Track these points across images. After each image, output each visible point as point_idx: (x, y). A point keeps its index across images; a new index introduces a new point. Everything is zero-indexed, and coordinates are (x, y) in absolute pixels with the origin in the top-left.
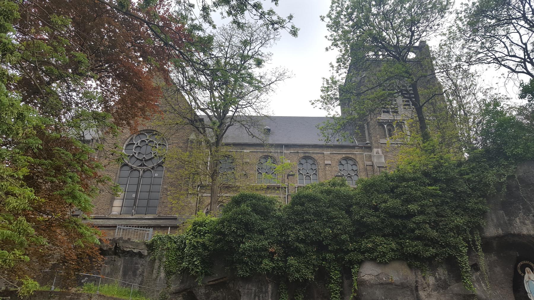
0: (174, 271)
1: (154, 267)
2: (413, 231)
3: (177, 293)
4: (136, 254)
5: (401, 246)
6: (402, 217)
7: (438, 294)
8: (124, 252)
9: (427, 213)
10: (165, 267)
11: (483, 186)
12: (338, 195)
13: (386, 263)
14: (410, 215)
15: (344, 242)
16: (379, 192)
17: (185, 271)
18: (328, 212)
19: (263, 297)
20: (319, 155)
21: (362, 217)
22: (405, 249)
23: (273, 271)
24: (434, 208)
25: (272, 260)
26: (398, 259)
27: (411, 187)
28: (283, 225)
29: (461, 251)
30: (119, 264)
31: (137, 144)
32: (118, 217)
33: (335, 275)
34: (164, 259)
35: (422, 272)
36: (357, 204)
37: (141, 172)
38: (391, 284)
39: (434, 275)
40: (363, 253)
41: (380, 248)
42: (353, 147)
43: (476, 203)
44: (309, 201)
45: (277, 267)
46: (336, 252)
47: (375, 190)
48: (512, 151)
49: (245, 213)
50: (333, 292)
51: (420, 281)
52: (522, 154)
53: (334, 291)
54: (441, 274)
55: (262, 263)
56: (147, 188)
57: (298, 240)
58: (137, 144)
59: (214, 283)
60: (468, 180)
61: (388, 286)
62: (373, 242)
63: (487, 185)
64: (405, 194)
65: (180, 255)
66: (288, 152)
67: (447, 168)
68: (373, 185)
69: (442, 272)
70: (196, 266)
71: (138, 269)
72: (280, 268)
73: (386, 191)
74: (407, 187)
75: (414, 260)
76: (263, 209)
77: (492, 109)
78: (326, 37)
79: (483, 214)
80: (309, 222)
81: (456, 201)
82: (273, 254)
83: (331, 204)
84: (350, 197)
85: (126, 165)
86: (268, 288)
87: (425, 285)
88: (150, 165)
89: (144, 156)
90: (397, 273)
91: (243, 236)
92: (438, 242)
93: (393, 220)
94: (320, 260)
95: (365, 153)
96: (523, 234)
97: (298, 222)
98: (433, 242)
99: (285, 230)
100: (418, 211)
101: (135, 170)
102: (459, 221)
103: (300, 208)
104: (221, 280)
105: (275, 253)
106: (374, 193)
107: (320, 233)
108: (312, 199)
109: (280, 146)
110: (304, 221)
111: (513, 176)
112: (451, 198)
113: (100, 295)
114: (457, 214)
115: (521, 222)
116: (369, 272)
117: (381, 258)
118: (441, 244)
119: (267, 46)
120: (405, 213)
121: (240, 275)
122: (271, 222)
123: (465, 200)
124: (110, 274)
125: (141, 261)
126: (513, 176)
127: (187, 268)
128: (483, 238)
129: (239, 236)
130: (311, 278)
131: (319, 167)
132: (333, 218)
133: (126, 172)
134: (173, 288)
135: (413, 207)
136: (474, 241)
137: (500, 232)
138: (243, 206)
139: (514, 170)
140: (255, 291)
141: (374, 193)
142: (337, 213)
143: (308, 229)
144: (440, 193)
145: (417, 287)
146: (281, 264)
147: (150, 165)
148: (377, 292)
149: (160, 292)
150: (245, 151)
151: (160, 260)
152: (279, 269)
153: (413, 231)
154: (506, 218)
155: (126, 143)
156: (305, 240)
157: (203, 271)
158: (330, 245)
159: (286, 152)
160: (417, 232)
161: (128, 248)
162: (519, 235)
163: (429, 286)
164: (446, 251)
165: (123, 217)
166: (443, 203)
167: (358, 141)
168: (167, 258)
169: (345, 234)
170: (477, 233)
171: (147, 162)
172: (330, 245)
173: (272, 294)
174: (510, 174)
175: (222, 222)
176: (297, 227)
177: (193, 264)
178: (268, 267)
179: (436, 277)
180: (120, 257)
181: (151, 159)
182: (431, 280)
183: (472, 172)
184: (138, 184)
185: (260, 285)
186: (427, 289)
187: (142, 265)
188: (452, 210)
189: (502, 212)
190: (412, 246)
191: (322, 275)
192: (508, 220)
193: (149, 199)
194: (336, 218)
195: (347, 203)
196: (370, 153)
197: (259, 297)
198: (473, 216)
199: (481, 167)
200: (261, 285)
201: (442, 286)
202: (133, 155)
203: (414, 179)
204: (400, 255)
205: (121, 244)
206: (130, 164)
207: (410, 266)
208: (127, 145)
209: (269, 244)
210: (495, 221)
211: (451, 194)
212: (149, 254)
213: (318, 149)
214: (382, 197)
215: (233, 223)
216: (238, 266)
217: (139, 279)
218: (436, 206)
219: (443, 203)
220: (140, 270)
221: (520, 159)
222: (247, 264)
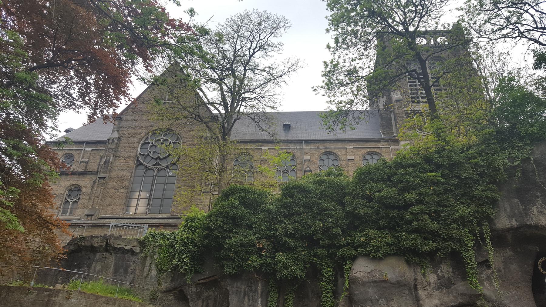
0: (166, 269)
1: (145, 264)
2: (410, 222)
3: (168, 291)
5: (398, 240)
6: (399, 208)
7: (440, 294)
8: (115, 249)
9: (426, 202)
10: (156, 264)
11: (493, 171)
12: (331, 185)
13: (380, 259)
14: (407, 205)
16: (373, 180)
17: (175, 268)
18: (319, 204)
19: (252, 297)
20: (342, 150)
21: (355, 208)
22: (402, 243)
23: (261, 268)
24: (435, 197)
25: (260, 256)
26: (394, 255)
27: (409, 174)
28: (273, 218)
29: (466, 245)
30: (110, 261)
31: (152, 143)
32: (132, 217)
33: (327, 272)
34: (156, 257)
35: (421, 269)
36: (350, 194)
37: (156, 171)
38: (385, 282)
39: (435, 272)
40: (356, 248)
41: (374, 243)
42: (379, 141)
43: (483, 191)
44: (299, 193)
45: (266, 264)
47: (369, 179)
48: (527, 130)
49: (232, 207)
50: (324, 291)
51: (419, 278)
52: (538, 133)
53: (326, 290)
54: (445, 271)
55: (249, 260)
56: (161, 187)
57: (286, 235)
58: (152, 143)
59: (205, 281)
60: (476, 164)
61: (382, 284)
62: (366, 235)
63: (497, 170)
64: (402, 182)
65: (172, 252)
66: (308, 148)
67: (450, 151)
68: (367, 173)
69: (446, 270)
70: (185, 263)
71: (130, 266)
72: (268, 265)
73: (383, 180)
74: (405, 174)
75: (412, 256)
76: (251, 201)
77: (507, 84)
78: (327, 17)
79: (494, 203)
80: (299, 215)
81: (461, 189)
82: (261, 249)
83: (323, 195)
84: (343, 187)
85: (142, 164)
86: (258, 286)
88: (164, 164)
89: (159, 155)
90: (393, 270)
91: (231, 231)
92: (439, 235)
93: (388, 211)
94: (311, 256)
95: (392, 147)
96: (542, 226)
97: (288, 215)
98: (434, 235)
99: (274, 224)
100: (416, 200)
102: (463, 210)
103: (289, 200)
104: (212, 279)
105: (263, 248)
106: (368, 181)
107: (311, 227)
108: (301, 190)
109: (300, 141)
110: (293, 214)
111: (528, 159)
112: (455, 185)
113: (80, 292)
114: (463, 203)
115: (538, 212)
116: (362, 269)
117: (374, 253)
118: (443, 238)
119: (278, 36)
120: (401, 203)
121: (226, 272)
122: (260, 216)
123: (472, 187)
124: (100, 272)
125: (133, 258)
126: (528, 159)
127: (177, 266)
128: (493, 231)
129: (226, 231)
130: (301, 276)
131: (342, 163)
132: (325, 211)
133: (141, 171)
134: (164, 286)
135: (410, 196)
136: (482, 234)
137: (514, 223)
138: (232, 199)
139: (530, 152)
140: (245, 290)
141: (368, 181)
142: (329, 204)
143: (297, 222)
144: (443, 180)
145: (416, 285)
146: (269, 260)
147: (164, 164)
148: (370, 291)
149: (151, 290)
150: (263, 148)
151: (152, 257)
152: (268, 266)
153: (410, 222)
154: (521, 207)
155: (142, 142)
156: (294, 234)
157: (193, 269)
158: (321, 239)
159: (305, 148)
160: (414, 223)
161: (119, 245)
162: (536, 227)
163: (429, 284)
164: (448, 245)
165: (137, 217)
166: (446, 191)
167: (384, 134)
168: (159, 256)
169: (337, 226)
170: (486, 225)
171: (162, 161)
172: (321, 239)
173: (262, 293)
174: (525, 156)
175: (210, 217)
176: (286, 221)
177: (183, 261)
178: (255, 264)
179: (438, 275)
180: (111, 254)
181: (165, 158)
182: (432, 278)
183: (481, 156)
184: (153, 183)
185: (250, 284)
186: (427, 287)
187: (134, 264)
188: (457, 199)
189: (516, 200)
190: (409, 240)
191: (314, 272)
192: (524, 209)
193: (163, 198)
194: (327, 210)
195: (339, 194)
196: (397, 147)
197: (249, 296)
198: (480, 205)
199: (490, 149)
200: (251, 283)
201: (445, 285)
202: (148, 155)
203: (413, 165)
204: (396, 250)
205: (111, 241)
206: (145, 163)
207: (408, 262)
208: (143, 145)
209: (257, 239)
210: (509, 210)
211: (455, 181)
212: (141, 251)
213: (340, 144)
214: (377, 186)
215: (220, 217)
216: (225, 263)
217: (130, 277)
218: (438, 195)
219: (446, 191)
220: (132, 268)
221: (535, 140)
222: (234, 260)
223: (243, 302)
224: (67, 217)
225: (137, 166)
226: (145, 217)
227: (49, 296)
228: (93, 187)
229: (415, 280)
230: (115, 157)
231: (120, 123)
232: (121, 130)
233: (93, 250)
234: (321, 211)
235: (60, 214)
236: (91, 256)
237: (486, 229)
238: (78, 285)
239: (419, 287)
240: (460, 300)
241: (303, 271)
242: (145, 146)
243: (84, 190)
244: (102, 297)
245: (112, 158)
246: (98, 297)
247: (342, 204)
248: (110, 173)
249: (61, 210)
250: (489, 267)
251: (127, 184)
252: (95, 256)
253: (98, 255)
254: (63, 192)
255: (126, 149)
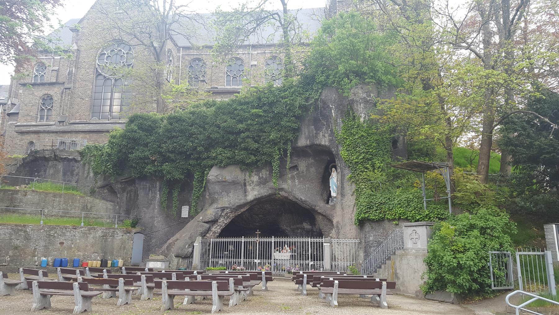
3: (102, 187)
4: (71, 160)
8: (62, 158)
13: (225, 167)
15: (200, 153)
16: (224, 114)
39: (258, 175)
46: (197, 159)
66: (256, 52)
71: (74, 170)
87: (250, 182)
101: (108, 79)
103: (170, 127)
105: (155, 160)
125: (76, 165)
134: (100, 183)
137: (308, 143)
143: (176, 143)
148: (217, 187)
151: (89, 164)
162: (320, 145)
172: (192, 154)
182: (255, 178)
190: (240, 155)
191: (189, 175)
194: (195, 134)
205: (58, 153)
206: (103, 74)
208: (99, 57)
210: (307, 134)
211: (271, 115)
212: (82, 159)
223: (148, 194)
224: (44, 123)
225: (97, 76)
226: (108, 122)
227: (12, 194)
228: (62, 97)
229: (245, 180)
230: (77, 68)
231: (78, 35)
232: (79, 42)
233: (46, 159)
234: (191, 135)
235: (39, 120)
236: (46, 163)
237: (289, 147)
238: (35, 186)
239: (247, 184)
240: (270, 192)
241: (182, 174)
242: (101, 58)
243: (55, 98)
244: (50, 193)
245: (74, 69)
246: (47, 194)
247: (205, 129)
248: (74, 83)
249: (39, 116)
250: (298, 170)
251: (90, 94)
252: (48, 164)
253: (50, 163)
254: (37, 101)
255: (86, 60)
